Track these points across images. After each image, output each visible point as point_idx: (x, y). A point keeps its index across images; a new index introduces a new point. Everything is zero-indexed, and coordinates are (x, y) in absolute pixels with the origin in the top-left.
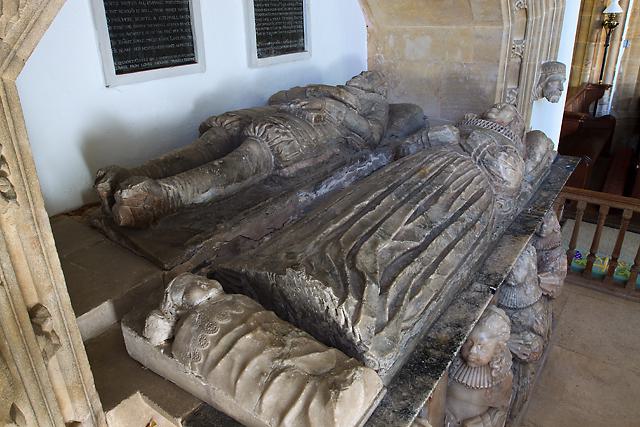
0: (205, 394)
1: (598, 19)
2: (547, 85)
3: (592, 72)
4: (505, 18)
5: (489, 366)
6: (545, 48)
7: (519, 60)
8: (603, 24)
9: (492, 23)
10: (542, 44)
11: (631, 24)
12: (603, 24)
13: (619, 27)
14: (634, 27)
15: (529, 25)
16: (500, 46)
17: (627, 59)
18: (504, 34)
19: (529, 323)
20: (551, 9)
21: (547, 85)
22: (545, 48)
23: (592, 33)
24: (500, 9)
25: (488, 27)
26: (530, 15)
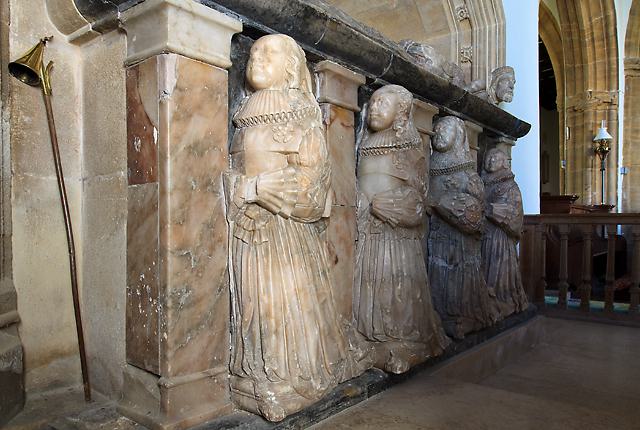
0: (310, 402)
1: (590, 146)
2: (498, 86)
3: (594, 197)
4: (451, 25)
5: (390, 126)
6: (493, 56)
7: (469, 64)
8: (596, 152)
9: (439, 32)
10: (490, 52)
11: (625, 153)
12: (596, 152)
13: (613, 152)
14: (629, 156)
15: (474, 35)
16: (450, 50)
17: (629, 187)
18: (453, 40)
19: (463, 186)
20: (493, 25)
21: (498, 86)
22: (493, 56)
23: (587, 160)
24: (445, 15)
25: (438, 37)
26: (474, 25)
